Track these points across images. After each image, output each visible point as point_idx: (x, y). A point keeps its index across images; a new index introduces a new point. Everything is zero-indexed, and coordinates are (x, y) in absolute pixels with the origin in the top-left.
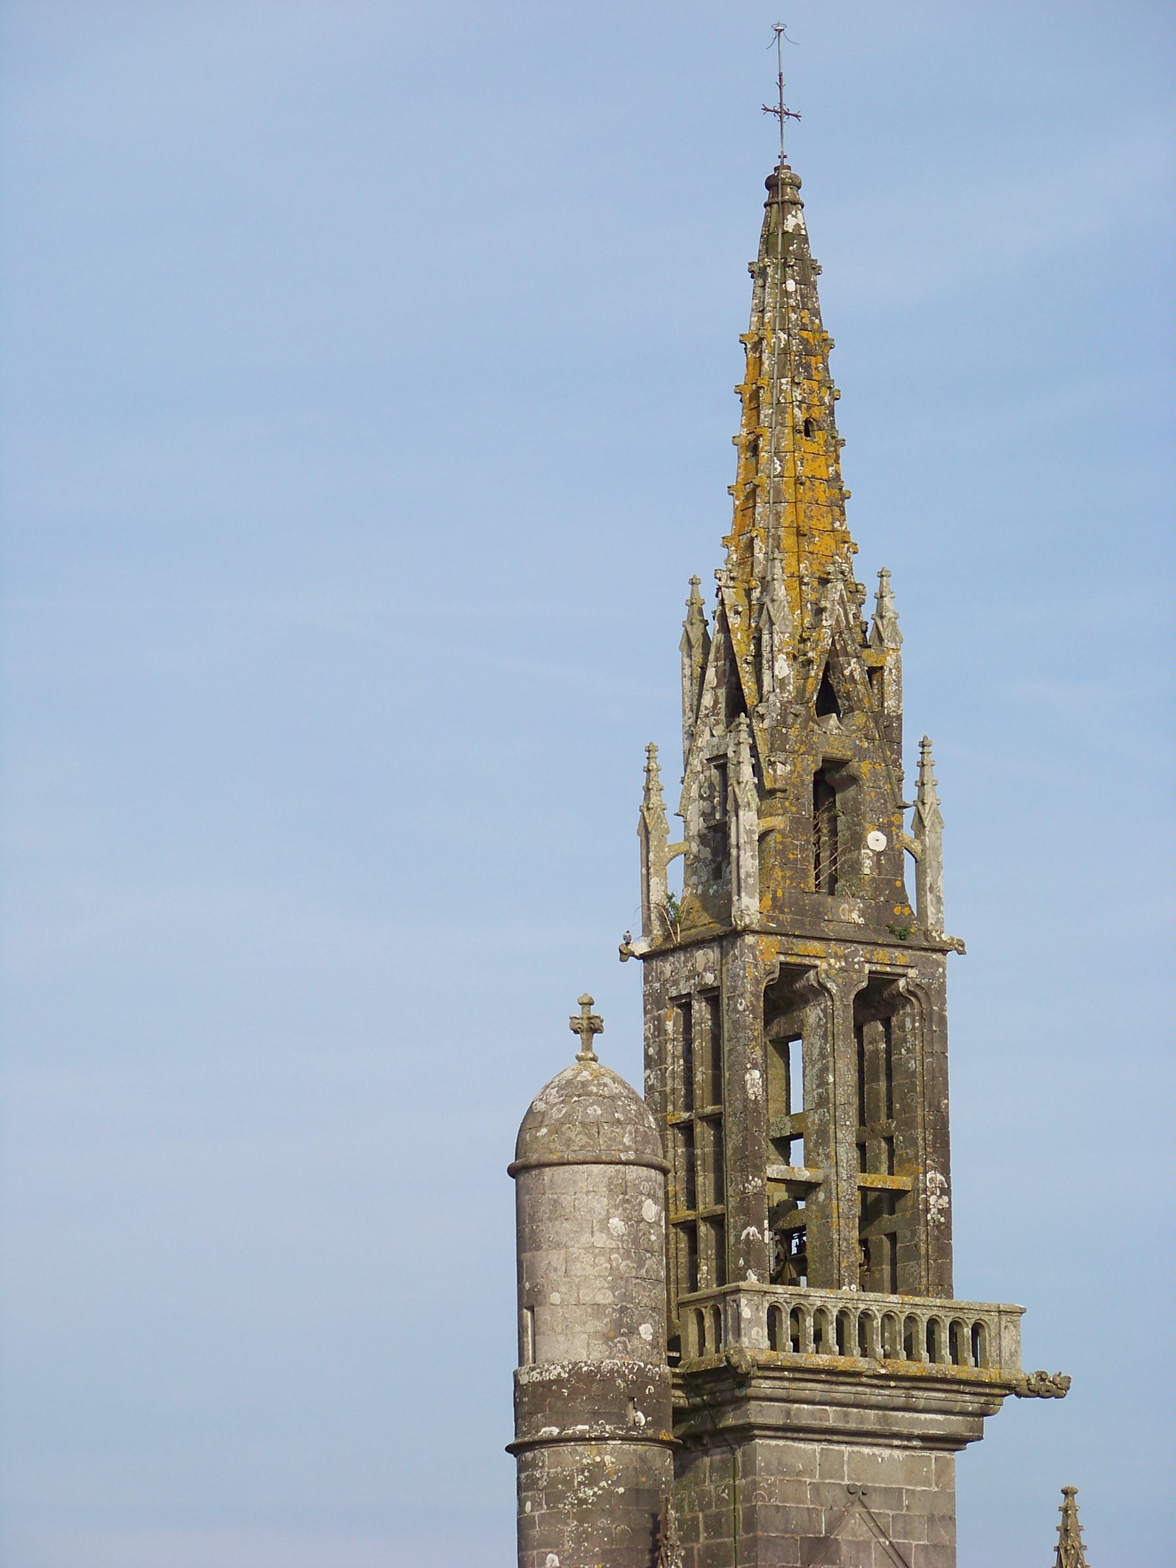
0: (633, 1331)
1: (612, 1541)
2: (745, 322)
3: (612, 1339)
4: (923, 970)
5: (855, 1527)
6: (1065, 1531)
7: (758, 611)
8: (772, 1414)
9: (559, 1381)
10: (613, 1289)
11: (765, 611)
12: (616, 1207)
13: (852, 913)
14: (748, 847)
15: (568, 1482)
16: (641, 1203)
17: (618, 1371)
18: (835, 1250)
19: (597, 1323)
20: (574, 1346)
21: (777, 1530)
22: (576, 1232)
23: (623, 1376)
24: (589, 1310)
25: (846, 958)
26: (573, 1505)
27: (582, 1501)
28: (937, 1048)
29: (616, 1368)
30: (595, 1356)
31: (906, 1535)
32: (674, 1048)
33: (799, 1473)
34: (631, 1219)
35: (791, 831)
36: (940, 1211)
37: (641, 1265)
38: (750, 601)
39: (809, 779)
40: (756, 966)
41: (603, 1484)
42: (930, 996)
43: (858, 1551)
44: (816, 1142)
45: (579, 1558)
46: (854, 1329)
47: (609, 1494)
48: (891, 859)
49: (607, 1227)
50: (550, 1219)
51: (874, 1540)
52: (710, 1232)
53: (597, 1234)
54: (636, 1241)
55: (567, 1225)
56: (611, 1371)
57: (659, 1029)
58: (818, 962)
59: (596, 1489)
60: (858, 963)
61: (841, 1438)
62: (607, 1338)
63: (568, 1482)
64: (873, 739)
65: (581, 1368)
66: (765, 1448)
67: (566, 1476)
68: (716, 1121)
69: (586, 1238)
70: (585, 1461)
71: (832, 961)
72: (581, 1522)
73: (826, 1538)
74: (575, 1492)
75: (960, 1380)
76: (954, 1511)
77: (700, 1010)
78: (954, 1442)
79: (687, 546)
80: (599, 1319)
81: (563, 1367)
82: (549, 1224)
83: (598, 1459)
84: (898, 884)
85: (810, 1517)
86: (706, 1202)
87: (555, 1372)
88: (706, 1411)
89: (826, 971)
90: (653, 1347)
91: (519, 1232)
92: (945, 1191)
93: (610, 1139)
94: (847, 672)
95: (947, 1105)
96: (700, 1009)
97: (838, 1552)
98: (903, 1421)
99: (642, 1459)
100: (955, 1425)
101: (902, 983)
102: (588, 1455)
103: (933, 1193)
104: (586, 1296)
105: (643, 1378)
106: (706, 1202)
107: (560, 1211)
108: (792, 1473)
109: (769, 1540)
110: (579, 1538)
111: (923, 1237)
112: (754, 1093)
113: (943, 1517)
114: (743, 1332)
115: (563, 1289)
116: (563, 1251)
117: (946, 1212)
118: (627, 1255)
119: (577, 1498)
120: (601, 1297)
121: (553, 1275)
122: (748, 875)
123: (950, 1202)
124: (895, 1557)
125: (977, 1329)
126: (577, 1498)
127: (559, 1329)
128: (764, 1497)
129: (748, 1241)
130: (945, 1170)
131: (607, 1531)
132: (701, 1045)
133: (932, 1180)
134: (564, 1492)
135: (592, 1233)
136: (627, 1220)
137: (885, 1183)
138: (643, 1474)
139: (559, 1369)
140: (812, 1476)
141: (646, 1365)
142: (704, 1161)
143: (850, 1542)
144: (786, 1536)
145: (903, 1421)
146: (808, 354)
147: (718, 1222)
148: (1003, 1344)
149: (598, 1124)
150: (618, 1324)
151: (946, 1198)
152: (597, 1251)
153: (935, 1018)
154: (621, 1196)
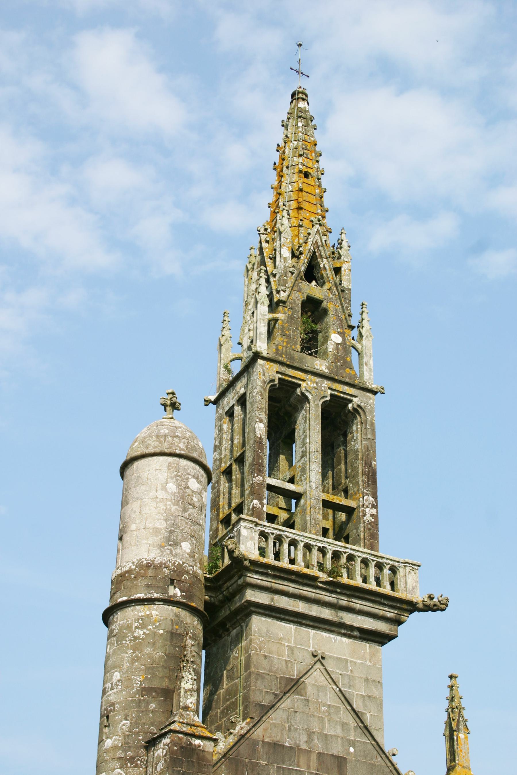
0: (177, 544)
1: (154, 662)
3: (163, 547)
4: (361, 399)
5: (316, 678)
6: (452, 699)
8: (263, 598)
9: (130, 571)
10: (166, 520)
11: (275, 220)
12: (172, 478)
13: (321, 365)
14: (262, 322)
15: (129, 627)
16: (187, 479)
17: (165, 564)
18: (308, 525)
19: (155, 538)
21: (265, 669)
22: (147, 491)
23: (167, 567)
24: (151, 531)
25: (317, 383)
26: (130, 640)
27: (136, 638)
28: (369, 436)
29: (164, 562)
30: (152, 557)
31: (350, 687)
33: (280, 639)
34: (181, 486)
35: (287, 322)
36: (372, 516)
37: (185, 510)
38: (406, 572)
39: (300, 302)
40: (264, 375)
41: (150, 627)
43: (318, 690)
45: (132, 672)
50: (134, 487)
51: (329, 686)
53: (159, 491)
54: (183, 497)
55: (143, 488)
56: (161, 563)
57: (221, 430)
58: (301, 382)
59: (145, 630)
60: (324, 387)
61: (308, 623)
62: (161, 547)
63: (129, 627)
64: (335, 295)
65: (143, 562)
66: (258, 623)
67: (128, 624)
69: (153, 494)
70: (140, 614)
71: (309, 383)
72: (135, 650)
74: (133, 633)
76: (381, 678)
77: (238, 410)
78: (381, 639)
80: (156, 536)
81: (133, 563)
82: (134, 489)
83: (148, 613)
84: (348, 359)
85: (287, 665)
87: (128, 566)
88: (221, 604)
89: (305, 387)
90: (191, 557)
91: (122, 504)
92: (375, 506)
93: (172, 444)
94: (322, 266)
95: (375, 465)
96: (386, 571)
97: (305, 689)
99: (177, 616)
101: (350, 406)
102: (141, 611)
103: (367, 507)
105: (180, 570)
107: (140, 481)
108: (271, 643)
109: (258, 674)
110: (133, 661)
111: (362, 529)
112: (260, 434)
113: (374, 681)
114: (241, 542)
115: (137, 521)
116: (140, 501)
117: (375, 517)
118: (176, 503)
119: (134, 637)
120: (158, 524)
121: (133, 516)
122: (261, 334)
123: (377, 512)
124: (343, 699)
125: (393, 570)
126: (134, 637)
127: (133, 543)
128: (256, 648)
129: (253, 507)
130: (375, 495)
131: (150, 656)
133: (367, 500)
134: (126, 634)
135: (157, 491)
136: (178, 485)
137: (341, 501)
138: (177, 624)
139: (131, 564)
140: (289, 641)
141: (183, 563)
142: (236, 482)
143: (313, 685)
144: (271, 674)
145: (349, 619)
146: (309, 150)
148: (408, 580)
149: (165, 436)
150: (168, 539)
151: (375, 510)
152: (158, 500)
153: (368, 423)
154: (175, 473)
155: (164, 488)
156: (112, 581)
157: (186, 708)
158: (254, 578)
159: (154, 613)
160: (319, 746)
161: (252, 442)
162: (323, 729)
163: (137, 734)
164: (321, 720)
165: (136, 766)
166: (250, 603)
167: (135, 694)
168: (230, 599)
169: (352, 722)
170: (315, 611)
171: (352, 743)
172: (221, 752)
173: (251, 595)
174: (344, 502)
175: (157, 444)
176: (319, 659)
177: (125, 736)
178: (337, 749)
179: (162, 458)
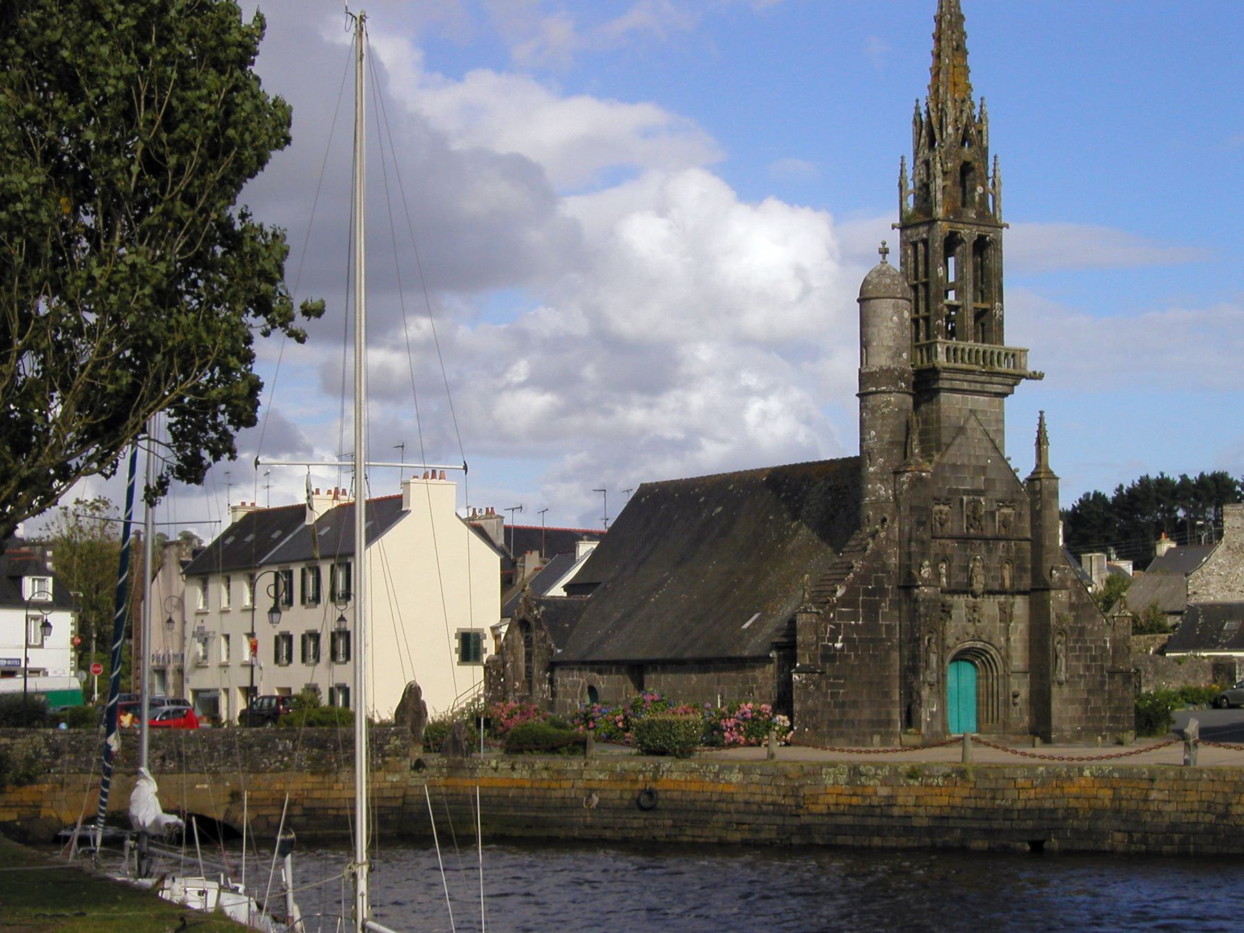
2: (935, 11)
5: (972, 423)
7: (942, 112)
15: (879, 407)
20: (881, 360)
32: (911, 260)
42: (997, 243)
46: (973, 355)
47: (892, 410)
48: (984, 197)
49: (893, 318)
52: (923, 328)
62: (893, 358)
66: (943, 396)
68: (926, 285)
75: (1006, 374)
79: (920, 89)
86: (922, 311)
88: (924, 385)
96: (920, 246)
100: (999, 388)
102: (885, 397)
106: (922, 311)
108: (951, 405)
125: (1013, 356)
132: (921, 258)
147: (927, 319)
156: (917, 122)
158: (945, 375)
160: (973, 461)
169: (989, 446)
171: (989, 458)
178: (982, 463)
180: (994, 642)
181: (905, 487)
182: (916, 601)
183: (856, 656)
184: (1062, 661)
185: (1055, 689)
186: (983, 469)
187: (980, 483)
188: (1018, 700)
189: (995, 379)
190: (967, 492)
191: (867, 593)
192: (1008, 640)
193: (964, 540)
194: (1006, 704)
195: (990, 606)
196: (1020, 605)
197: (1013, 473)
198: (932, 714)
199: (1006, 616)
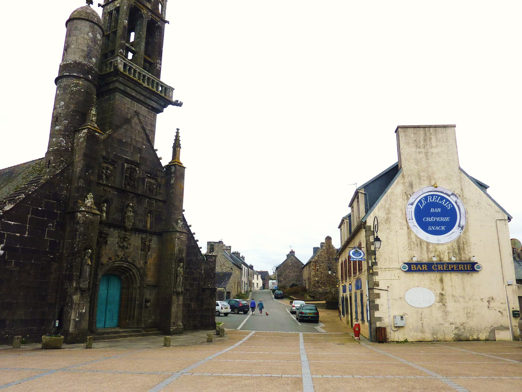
5: (135, 120)
8: (122, 87)
9: (71, 64)
10: (87, 48)
15: (69, 86)
23: (87, 66)
27: (72, 90)
30: (81, 60)
44: (125, 184)
47: (79, 90)
54: (95, 40)
62: (84, 57)
63: (69, 86)
66: (118, 96)
73: (129, 119)
98: (149, 102)
104: (80, 47)
105: (91, 69)
110: (70, 99)
118: (92, 42)
145: (149, 102)
155: (87, 34)
157: (92, 121)
159: (80, 82)
161: (122, 27)
162: (136, 138)
163: (71, 127)
164: (136, 135)
165: (70, 138)
166: (117, 88)
167: (70, 112)
168: (108, 84)
170: (138, 96)
172: (463, 259)
173: (117, 85)
174: (150, 60)
175: (85, 15)
176: (137, 113)
177: (65, 127)
178: (139, 146)
179: (87, 22)
180: (136, 263)
181: (82, 139)
182: (78, 223)
183: (16, 264)
184: (180, 279)
185: (174, 297)
186: (140, 150)
187: (137, 158)
188: (148, 304)
189: (153, 97)
190: (127, 161)
191: (35, 212)
192: (146, 263)
193: (122, 192)
194: (140, 306)
195: (135, 240)
196: (154, 243)
197: (159, 159)
198: (81, 315)
199: (145, 248)
